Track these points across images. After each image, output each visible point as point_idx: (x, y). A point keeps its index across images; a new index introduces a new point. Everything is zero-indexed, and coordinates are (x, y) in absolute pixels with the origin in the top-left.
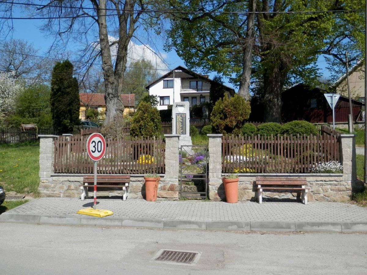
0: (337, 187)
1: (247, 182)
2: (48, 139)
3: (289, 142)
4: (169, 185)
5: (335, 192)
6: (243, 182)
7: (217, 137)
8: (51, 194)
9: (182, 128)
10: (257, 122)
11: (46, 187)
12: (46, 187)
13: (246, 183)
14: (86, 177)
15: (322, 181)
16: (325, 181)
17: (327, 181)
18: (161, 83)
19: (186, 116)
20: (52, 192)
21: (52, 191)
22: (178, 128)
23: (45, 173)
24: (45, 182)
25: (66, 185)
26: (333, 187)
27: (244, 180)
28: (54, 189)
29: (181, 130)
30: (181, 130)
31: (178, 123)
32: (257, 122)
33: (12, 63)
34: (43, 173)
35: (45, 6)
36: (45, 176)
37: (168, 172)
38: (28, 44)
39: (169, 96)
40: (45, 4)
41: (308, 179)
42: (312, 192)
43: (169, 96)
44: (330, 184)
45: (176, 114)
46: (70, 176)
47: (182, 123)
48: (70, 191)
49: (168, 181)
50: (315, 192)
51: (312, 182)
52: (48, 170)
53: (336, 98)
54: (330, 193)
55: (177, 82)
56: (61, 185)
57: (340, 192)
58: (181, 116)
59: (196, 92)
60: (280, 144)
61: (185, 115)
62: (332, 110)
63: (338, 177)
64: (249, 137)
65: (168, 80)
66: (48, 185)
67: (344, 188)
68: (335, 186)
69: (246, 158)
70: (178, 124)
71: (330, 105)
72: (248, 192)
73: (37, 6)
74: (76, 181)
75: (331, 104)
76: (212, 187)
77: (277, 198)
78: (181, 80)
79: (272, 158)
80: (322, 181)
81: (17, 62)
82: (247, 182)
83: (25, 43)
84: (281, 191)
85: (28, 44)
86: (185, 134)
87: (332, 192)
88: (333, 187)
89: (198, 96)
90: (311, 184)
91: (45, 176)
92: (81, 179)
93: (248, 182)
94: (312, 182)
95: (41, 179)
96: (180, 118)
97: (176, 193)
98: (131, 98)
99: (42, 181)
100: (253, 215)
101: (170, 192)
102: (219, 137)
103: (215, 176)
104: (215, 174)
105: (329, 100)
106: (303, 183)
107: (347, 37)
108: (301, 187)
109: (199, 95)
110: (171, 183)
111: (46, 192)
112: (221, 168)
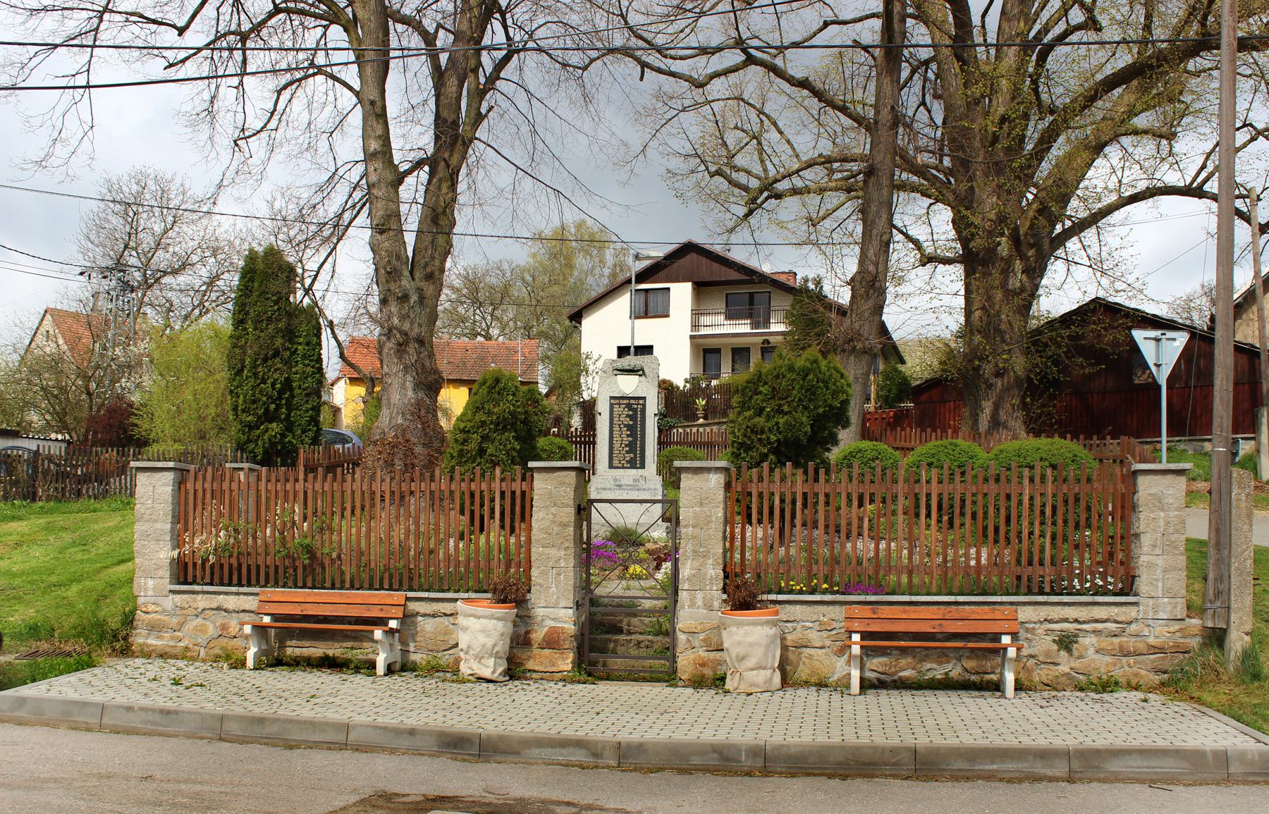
0: (1116, 640)
1: (807, 624)
2: (160, 475)
3: (959, 488)
4: (546, 629)
5: (1108, 659)
6: (794, 624)
7: (709, 470)
8: (168, 650)
9: (632, 447)
10: (929, 430)
11: (154, 628)
12: (154, 628)
13: (803, 626)
14: (263, 598)
15: (1066, 620)
16: (1076, 621)
17: (1084, 622)
18: (623, 303)
19: (644, 406)
20: (172, 643)
21: (172, 638)
22: (617, 445)
23: (151, 583)
24: (150, 609)
25: (214, 623)
26: (1106, 643)
27: (799, 617)
28: (179, 634)
29: (627, 452)
30: (627, 452)
31: (616, 428)
32: (929, 430)
33: (132, 244)
34: (145, 584)
35: (199, 50)
36: (150, 593)
37: (541, 585)
38: (178, 181)
39: (651, 347)
40: (201, 45)
41: (1025, 614)
42: (1032, 656)
43: (651, 347)
44: (1094, 632)
45: (612, 398)
46: (226, 593)
47: (631, 429)
48: (224, 641)
49: (540, 618)
50: (1041, 658)
51: (1031, 626)
52: (160, 573)
53: (1176, 344)
54: (1093, 661)
55: (681, 294)
56: (199, 621)
57: (1124, 660)
58: (629, 406)
59: (747, 329)
60: (928, 495)
61: (641, 402)
62: (1159, 387)
63: (1123, 609)
64: (822, 471)
65: (646, 291)
66: (159, 620)
67: (1141, 646)
68: (1110, 639)
69: (911, 554)
70: (616, 434)
71: (1154, 369)
72: (810, 657)
73: (166, 53)
74: (244, 611)
75: (1155, 365)
76: (688, 640)
77: (908, 678)
78: (694, 289)
79: (809, 523)
80: (1066, 620)
81: (147, 241)
82: (807, 624)
83: (168, 176)
84: (926, 654)
85: (178, 181)
86: (643, 467)
87: (1098, 657)
88: (1106, 643)
89: (755, 344)
90: (1027, 630)
91: (150, 593)
92: (251, 603)
93: (811, 625)
94: (1031, 626)
95: (141, 600)
96: (622, 412)
97: (567, 658)
98: (523, 355)
99: (144, 609)
100: (705, 712)
101: (547, 652)
102: (717, 469)
103: (700, 602)
104: (699, 595)
105: (1148, 350)
106: (1006, 626)
107: (1261, 138)
108: (999, 640)
109: (760, 339)
110: (552, 624)
111: (154, 642)
112: (722, 575)
